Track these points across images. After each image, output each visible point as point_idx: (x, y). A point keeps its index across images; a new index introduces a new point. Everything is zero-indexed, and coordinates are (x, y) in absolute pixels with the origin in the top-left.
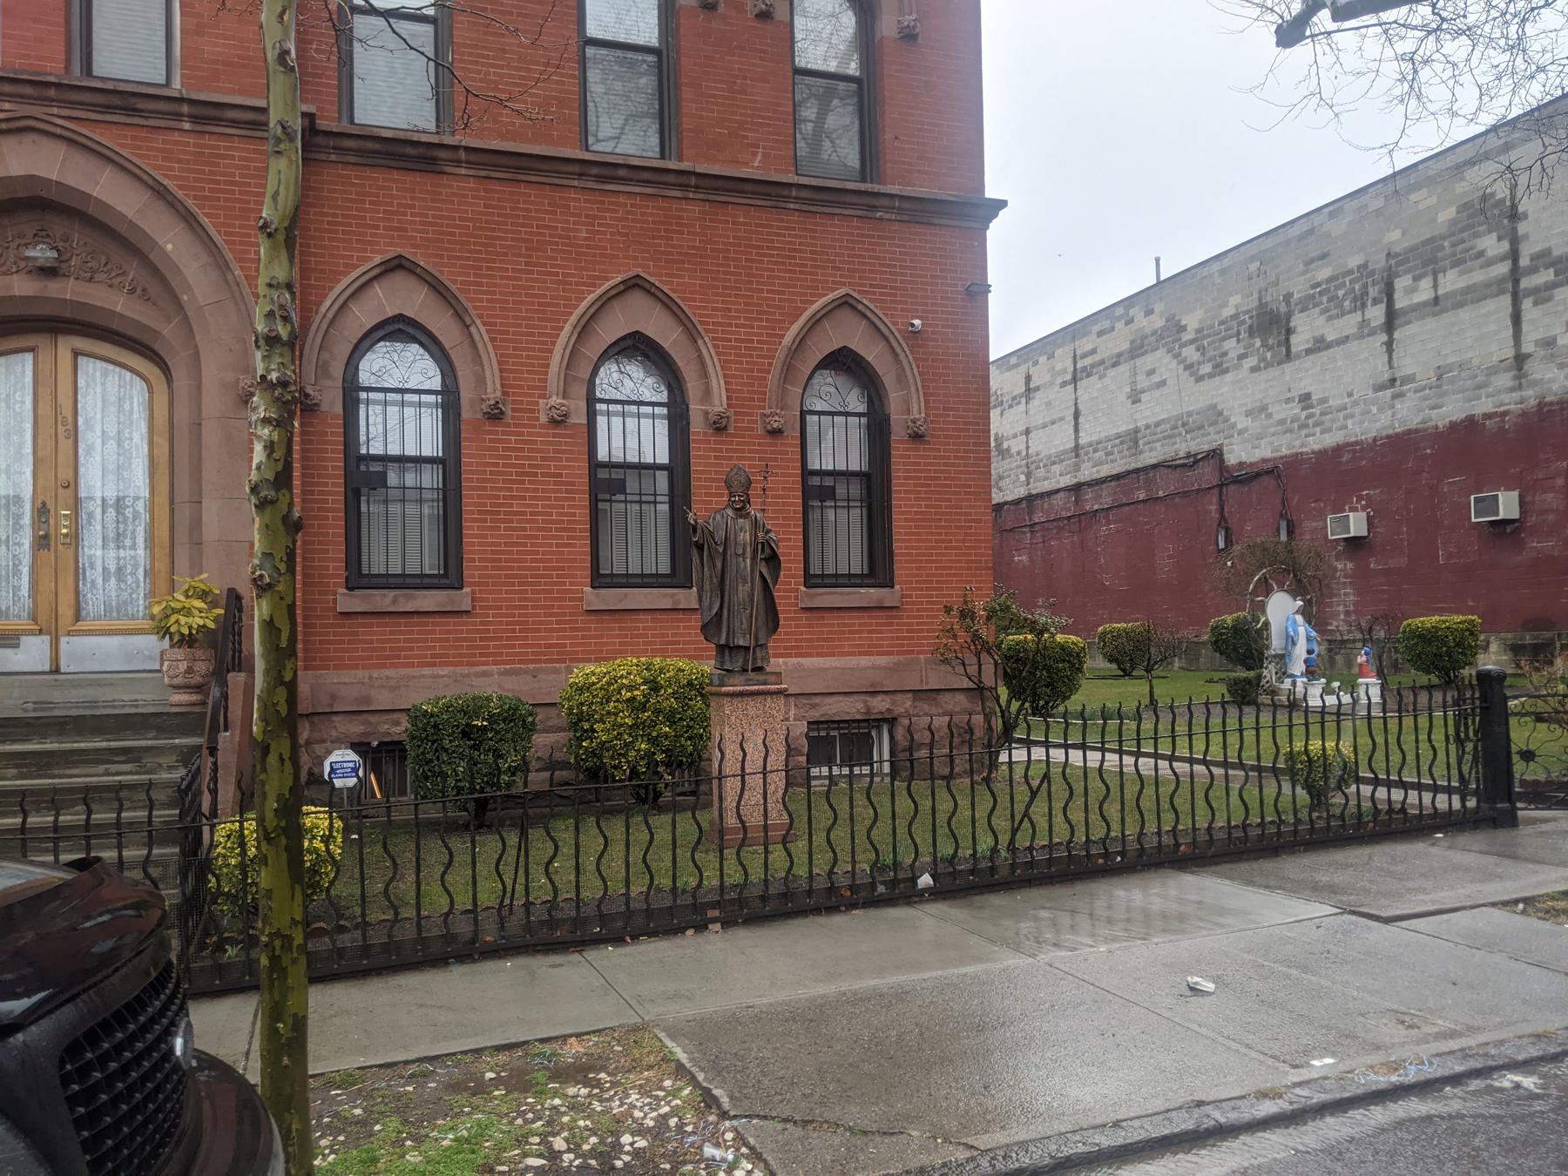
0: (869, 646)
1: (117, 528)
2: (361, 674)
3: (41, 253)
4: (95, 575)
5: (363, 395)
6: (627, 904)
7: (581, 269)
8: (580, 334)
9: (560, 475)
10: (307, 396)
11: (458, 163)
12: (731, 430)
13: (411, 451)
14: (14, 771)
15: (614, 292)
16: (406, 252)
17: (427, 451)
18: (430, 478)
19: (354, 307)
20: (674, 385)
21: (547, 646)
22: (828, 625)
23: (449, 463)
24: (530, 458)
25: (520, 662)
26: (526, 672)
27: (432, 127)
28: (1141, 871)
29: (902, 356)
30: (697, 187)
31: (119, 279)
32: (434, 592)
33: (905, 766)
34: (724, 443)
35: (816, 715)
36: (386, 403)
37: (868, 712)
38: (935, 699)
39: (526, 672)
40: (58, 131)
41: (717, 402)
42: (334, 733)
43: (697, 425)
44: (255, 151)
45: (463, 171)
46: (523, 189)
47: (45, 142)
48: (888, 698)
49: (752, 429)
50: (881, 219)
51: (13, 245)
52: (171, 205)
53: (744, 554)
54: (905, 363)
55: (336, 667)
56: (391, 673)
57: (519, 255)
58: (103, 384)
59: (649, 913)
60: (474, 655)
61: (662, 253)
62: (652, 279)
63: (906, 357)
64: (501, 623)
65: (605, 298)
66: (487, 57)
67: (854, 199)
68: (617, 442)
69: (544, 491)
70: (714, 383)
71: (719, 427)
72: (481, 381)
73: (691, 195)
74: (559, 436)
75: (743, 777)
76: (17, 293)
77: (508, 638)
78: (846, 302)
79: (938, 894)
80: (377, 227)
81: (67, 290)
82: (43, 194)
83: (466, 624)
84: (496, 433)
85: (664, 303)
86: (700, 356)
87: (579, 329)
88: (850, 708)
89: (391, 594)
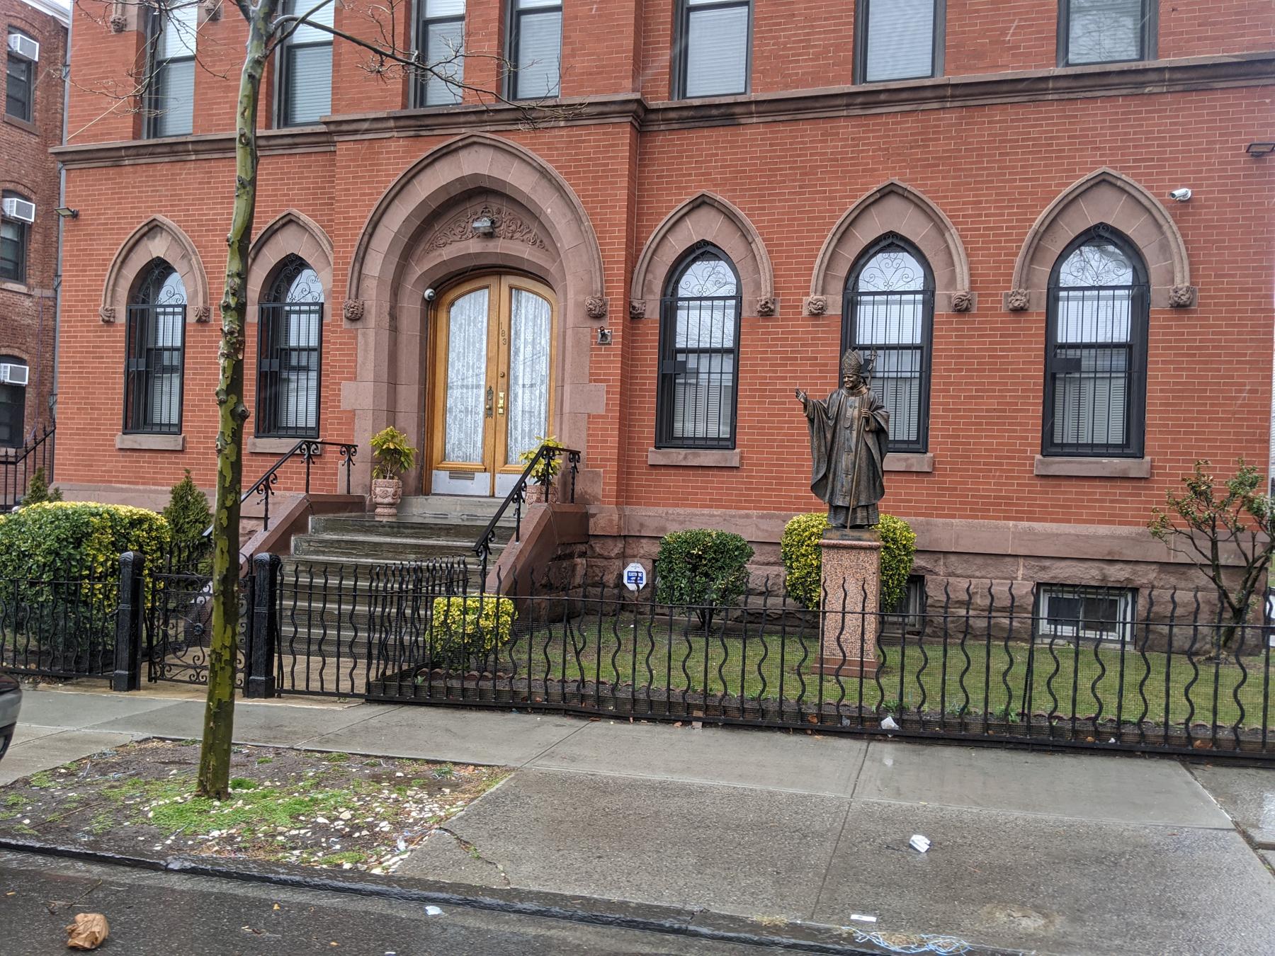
0: (1111, 515)
1: (531, 403)
2: (660, 510)
3: (484, 224)
4: (517, 434)
5: (1063, 294)
6: (742, 703)
7: (845, 184)
8: (839, 240)
9: (816, 358)
10: (634, 308)
11: (750, 114)
12: (974, 311)
13: (893, 340)
14: (413, 556)
15: (871, 200)
16: (896, 180)
17: (907, 340)
18: (909, 364)
19: (670, 238)
20: (1139, 267)
21: (796, 497)
22: (1065, 493)
23: (925, 349)
24: (792, 346)
25: (775, 509)
26: (778, 517)
27: (1133, 53)
28: (1140, 757)
29: (1165, 227)
30: (952, 96)
31: (528, 236)
32: (714, 451)
33: (1145, 636)
34: (965, 323)
35: (1045, 577)
36: (1083, 298)
37: (1104, 578)
38: (1184, 573)
39: (778, 517)
40: (488, 142)
41: (959, 287)
42: (642, 552)
43: (942, 308)
44: (604, 134)
45: (755, 120)
46: (801, 126)
47: (483, 151)
48: (1128, 568)
49: (996, 309)
50: (1150, 94)
51: (471, 220)
52: (550, 180)
53: (851, 426)
54: (1169, 234)
55: (646, 504)
56: (680, 510)
57: (794, 181)
58: (526, 307)
59: (670, 705)
60: (740, 501)
61: (919, 160)
62: (903, 185)
63: (1170, 226)
64: (762, 477)
65: (862, 207)
66: (780, 24)
67: (1116, 80)
68: (694, 331)
69: (801, 372)
70: (958, 270)
71: (961, 309)
72: (758, 286)
73: (948, 105)
74: (817, 326)
75: (844, 614)
76: (471, 251)
77: (766, 490)
78: (1104, 180)
79: (900, 737)
80: (690, 175)
81: (500, 246)
82: (482, 185)
83: (736, 477)
84: (767, 327)
85: (917, 205)
86: (948, 247)
87: (838, 236)
88: (1088, 574)
89: (683, 452)
